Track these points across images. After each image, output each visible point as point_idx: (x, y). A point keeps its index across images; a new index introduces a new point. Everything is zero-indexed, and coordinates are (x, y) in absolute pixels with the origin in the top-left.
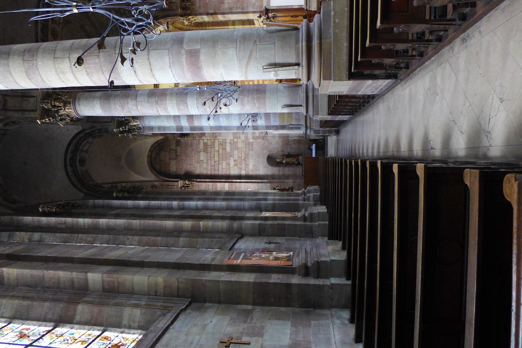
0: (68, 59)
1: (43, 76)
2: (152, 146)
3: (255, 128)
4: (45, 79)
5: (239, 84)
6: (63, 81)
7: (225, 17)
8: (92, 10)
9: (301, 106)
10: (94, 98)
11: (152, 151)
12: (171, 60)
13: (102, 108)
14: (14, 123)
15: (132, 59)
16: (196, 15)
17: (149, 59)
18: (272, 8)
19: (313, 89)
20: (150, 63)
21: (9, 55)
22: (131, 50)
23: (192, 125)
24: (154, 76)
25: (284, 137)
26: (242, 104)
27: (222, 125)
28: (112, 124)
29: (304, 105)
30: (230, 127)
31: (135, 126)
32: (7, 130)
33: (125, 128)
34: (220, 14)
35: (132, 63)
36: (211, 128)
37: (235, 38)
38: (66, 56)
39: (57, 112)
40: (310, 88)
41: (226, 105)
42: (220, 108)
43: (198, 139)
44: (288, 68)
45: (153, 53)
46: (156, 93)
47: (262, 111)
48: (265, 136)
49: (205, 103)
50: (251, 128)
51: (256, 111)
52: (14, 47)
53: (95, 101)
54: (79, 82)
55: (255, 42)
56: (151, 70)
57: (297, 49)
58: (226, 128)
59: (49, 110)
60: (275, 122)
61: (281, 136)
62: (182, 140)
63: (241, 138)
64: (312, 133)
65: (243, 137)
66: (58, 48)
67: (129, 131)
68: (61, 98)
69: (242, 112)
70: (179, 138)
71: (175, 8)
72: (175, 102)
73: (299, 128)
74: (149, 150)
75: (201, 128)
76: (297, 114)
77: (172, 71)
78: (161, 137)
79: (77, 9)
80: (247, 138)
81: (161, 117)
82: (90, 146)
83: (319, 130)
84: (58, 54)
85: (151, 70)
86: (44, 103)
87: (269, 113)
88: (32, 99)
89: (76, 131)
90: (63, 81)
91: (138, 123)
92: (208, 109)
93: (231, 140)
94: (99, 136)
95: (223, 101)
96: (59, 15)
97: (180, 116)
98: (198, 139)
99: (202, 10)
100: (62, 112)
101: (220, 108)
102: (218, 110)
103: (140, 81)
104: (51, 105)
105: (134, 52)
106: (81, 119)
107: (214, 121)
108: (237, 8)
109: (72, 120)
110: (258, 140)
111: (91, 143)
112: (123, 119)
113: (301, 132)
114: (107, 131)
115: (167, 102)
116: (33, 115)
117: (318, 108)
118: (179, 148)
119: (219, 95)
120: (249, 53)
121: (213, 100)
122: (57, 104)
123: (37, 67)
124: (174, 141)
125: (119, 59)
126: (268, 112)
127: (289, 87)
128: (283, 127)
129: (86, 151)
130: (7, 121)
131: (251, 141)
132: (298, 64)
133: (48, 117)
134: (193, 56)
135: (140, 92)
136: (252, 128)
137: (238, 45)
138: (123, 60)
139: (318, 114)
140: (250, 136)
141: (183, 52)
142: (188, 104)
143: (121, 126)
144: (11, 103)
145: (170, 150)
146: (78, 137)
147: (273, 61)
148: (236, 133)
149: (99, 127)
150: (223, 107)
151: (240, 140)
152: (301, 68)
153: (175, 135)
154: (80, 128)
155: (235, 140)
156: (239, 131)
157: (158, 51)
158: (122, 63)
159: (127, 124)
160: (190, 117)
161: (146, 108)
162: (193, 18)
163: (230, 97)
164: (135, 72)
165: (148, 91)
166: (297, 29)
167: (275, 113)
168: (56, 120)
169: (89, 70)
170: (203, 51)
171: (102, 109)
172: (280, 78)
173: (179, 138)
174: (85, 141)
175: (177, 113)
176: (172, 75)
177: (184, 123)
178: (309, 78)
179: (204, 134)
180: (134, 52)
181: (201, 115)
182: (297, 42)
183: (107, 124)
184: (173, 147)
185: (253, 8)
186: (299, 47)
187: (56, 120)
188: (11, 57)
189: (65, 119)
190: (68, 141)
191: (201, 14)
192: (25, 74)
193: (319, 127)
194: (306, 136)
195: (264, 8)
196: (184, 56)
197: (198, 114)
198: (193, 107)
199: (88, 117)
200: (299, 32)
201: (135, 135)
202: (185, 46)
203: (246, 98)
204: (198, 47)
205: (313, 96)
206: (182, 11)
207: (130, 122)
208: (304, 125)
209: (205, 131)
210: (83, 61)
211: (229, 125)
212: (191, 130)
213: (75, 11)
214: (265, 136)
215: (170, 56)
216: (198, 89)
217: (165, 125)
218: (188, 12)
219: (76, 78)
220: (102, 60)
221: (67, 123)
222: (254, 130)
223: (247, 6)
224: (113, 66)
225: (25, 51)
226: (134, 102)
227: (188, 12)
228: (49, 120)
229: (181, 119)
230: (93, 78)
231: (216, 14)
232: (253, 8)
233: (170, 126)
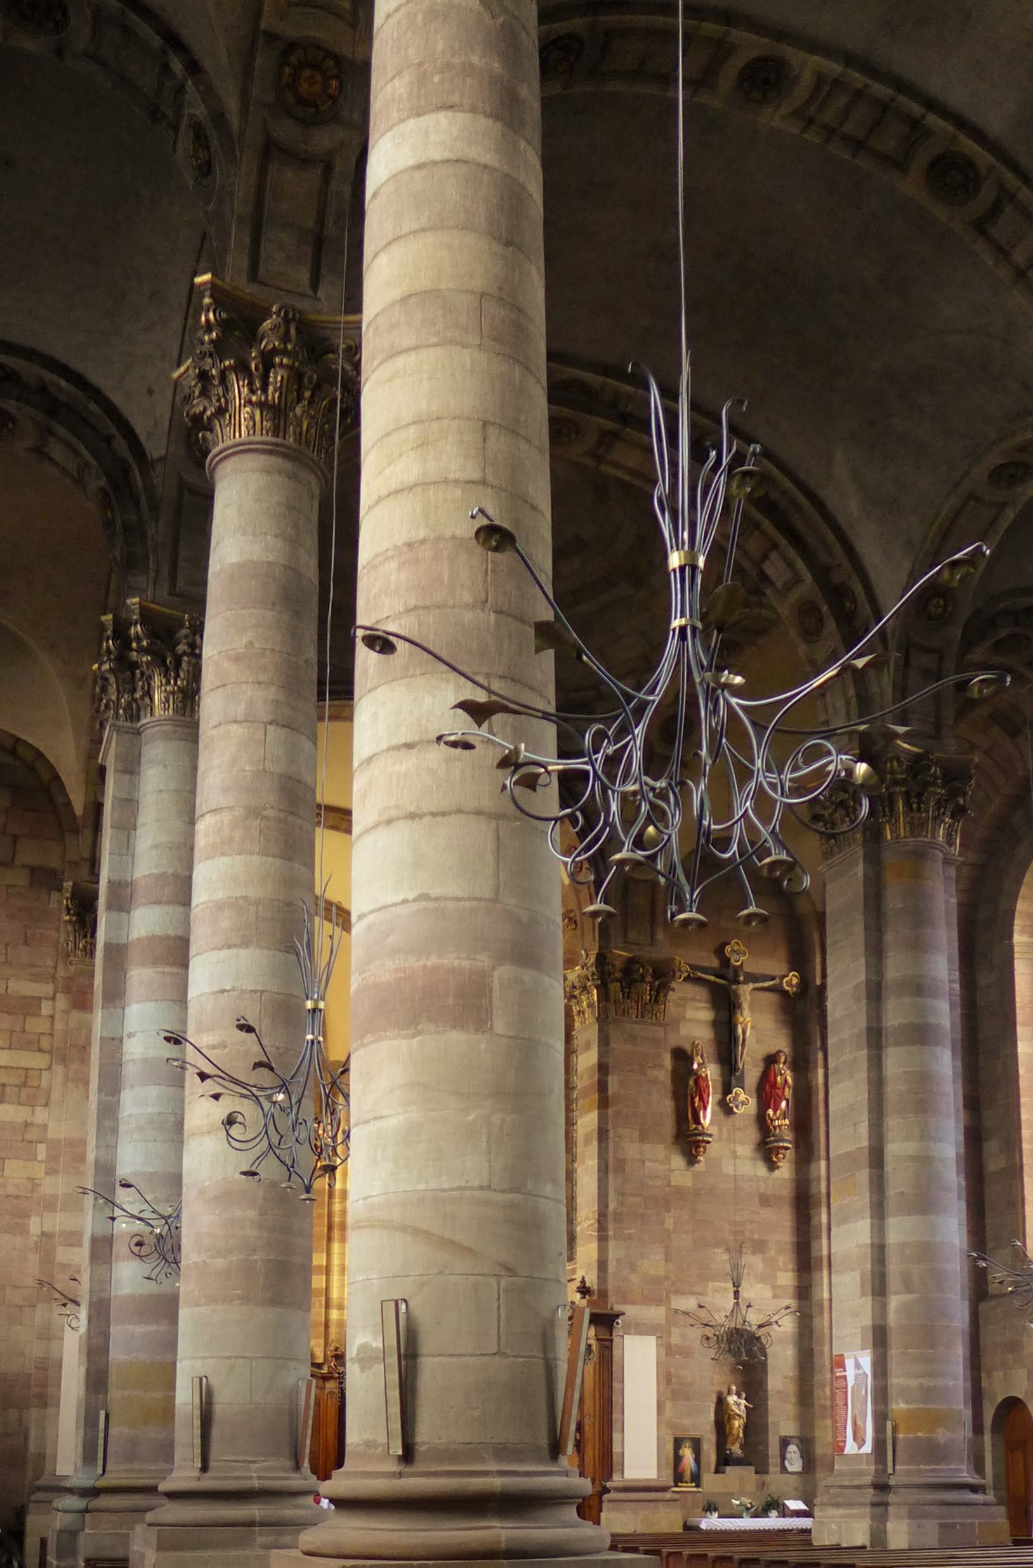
0: (476, 475)
1: (413, 358)
2: (40, 755)
3: (102, 1249)
4: (400, 362)
5: (322, 1183)
6: (388, 434)
7: (587, 1141)
8: (676, 623)
9: (204, 1468)
10: (294, 542)
11: (13, 752)
12: (451, 905)
13: (247, 568)
14: (206, 169)
15: (468, 746)
16: (603, 1020)
17: (459, 811)
18: (616, 1340)
19: (301, 1525)
20: (444, 814)
21: (508, 243)
22: (516, 751)
23: (134, 954)
24: (389, 822)
25: (44, 1384)
26: (225, 1197)
27: (128, 1098)
28: (163, 593)
29: (208, 1483)
30: (115, 1131)
31: (149, 694)
32: (175, 128)
33: (141, 650)
34: (603, 1119)
35: (454, 744)
36: (114, 1044)
37: (529, 1186)
38: (489, 470)
39: (242, 368)
40: (287, 1511)
41: (230, 1121)
42: (216, 1097)
43: (61, 973)
44: (395, 1410)
45: (481, 832)
46: (303, 815)
47: (187, 1287)
48: (54, 1291)
49: (249, 1029)
50: (102, 1230)
51: (189, 1256)
52: (534, 272)
53: (279, 544)
54: (379, 500)
55: (511, 1271)
56: (412, 816)
57: (472, 1451)
58: (109, 1112)
59: (252, 336)
60: (127, 1342)
61: (49, 1370)
62: (60, 901)
63: (49, 1180)
64: (60, 1521)
65: (56, 1185)
66: (524, 446)
67: (125, 667)
68: (300, 398)
69: (189, 1193)
70: (68, 885)
71: (632, 935)
72: (253, 893)
73: (88, 1456)
74: (18, 740)
75: (116, 995)
76: (166, 1451)
77: (405, 902)
78: (78, 801)
79: (682, 569)
80: (49, 1204)
81: (186, 817)
82: (64, 471)
83: (73, 1553)
84: (498, 442)
85: (412, 816)
86: (287, 321)
87: (174, 1319)
88: (303, 275)
89: (141, 427)
90: (388, 434)
91: (158, 711)
92: (210, 1035)
93: (45, 1126)
94: (108, 524)
95: (247, 1108)
96: (661, 490)
97: (189, 904)
98: (61, 973)
99: (618, 1045)
100: (239, 389)
101: (216, 1097)
102: (210, 1086)
103: (369, 761)
104: (275, 351)
105: (508, 762)
106: (202, 465)
107: (145, 1061)
108: (621, 1194)
109: (199, 423)
110: (34, 1259)
111: (79, 481)
112: (182, 648)
113: (67, 1460)
114: (132, 563)
115: (256, 859)
116: (237, 261)
117: (194, 1547)
118: (20, 879)
119: (281, 1097)
120: (467, 1243)
121: (258, 1065)
122: (277, 377)
123: (451, 342)
124: (54, 863)
125: (481, 697)
126: (184, 1314)
127: (293, 1414)
128: (97, 1380)
129: (40, 452)
130: (214, 143)
131: (35, 1225)
132: (408, 1455)
133: (225, 326)
134: (466, 1003)
135: (307, 745)
136: (100, 1233)
137: (500, 1197)
138: (477, 711)
139: (161, 1547)
140: (57, 1221)
141: (484, 961)
142: (242, 952)
143: (152, 634)
144: (294, 185)
145: (15, 838)
146: (113, 430)
147: (427, 1344)
148: (82, 1159)
149: (151, 531)
150: (220, 1111)
151: (39, 1171)
152: (393, 1467)
153: (85, 869)
154: (155, 449)
155: (42, 1150)
156: (90, 1170)
157: (490, 858)
158: (467, 706)
159: (160, 661)
160: (176, 953)
161: (234, 760)
162: (590, 1005)
163: (265, 1143)
164: (409, 746)
165: (307, 778)
166: (555, 1450)
167: (170, 1344)
168: (203, 355)
169: (426, 552)
170: (482, 1042)
171: (241, 566)
172: (354, 1374)
173: (68, 885)
174: (90, 458)
175: (201, 896)
176: (390, 900)
177: (146, 922)
178: (342, 1504)
179: (82, 1001)
180: (508, 762)
181: (185, 1002)
182: (503, 1452)
183: (165, 571)
184: (28, 854)
185: (619, 1261)
186: (482, 1460)
187: (203, 355)
188: (498, 248)
189: (205, 393)
190: (95, 376)
191: (604, 1041)
192: (425, 284)
193: (90, 1553)
194: (39, 1489)
195: (618, 1308)
196: (466, 964)
197: (192, 993)
198: (218, 974)
199: (208, 498)
200: (540, 1460)
201: (104, 690)
202: (504, 972)
203: (252, 1214)
204: (500, 1025)
205: (250, 1524)
206: (618, 963)
207: (166, 675)
208: (103, 1483)
209: (98, 1016)
210: (496, 549)
211: (123, 1128)
212: (108, 946)
213: (675, 560)
214: (54, 1291)
215: (468, 904)
216: (309, 1005)
217: (140, 832)
218: (614, 987)
219: (397, 492)
220: (468, 616)
221: (187, 399)
222: (94, 1240)
223: (630, 1237)
224: (444, 656)
225: (520, 311)
226: (263, 712)
227: (614, 987)
228: (209, 327)
229: (168, 909)
230: (392, 565)
231: (604, 1104)
232: (619, 1261)
233: (137, 851)
